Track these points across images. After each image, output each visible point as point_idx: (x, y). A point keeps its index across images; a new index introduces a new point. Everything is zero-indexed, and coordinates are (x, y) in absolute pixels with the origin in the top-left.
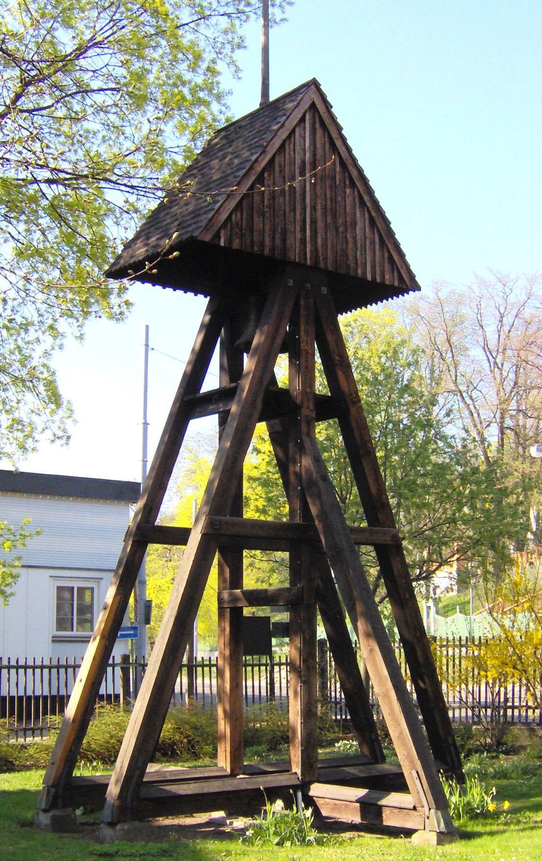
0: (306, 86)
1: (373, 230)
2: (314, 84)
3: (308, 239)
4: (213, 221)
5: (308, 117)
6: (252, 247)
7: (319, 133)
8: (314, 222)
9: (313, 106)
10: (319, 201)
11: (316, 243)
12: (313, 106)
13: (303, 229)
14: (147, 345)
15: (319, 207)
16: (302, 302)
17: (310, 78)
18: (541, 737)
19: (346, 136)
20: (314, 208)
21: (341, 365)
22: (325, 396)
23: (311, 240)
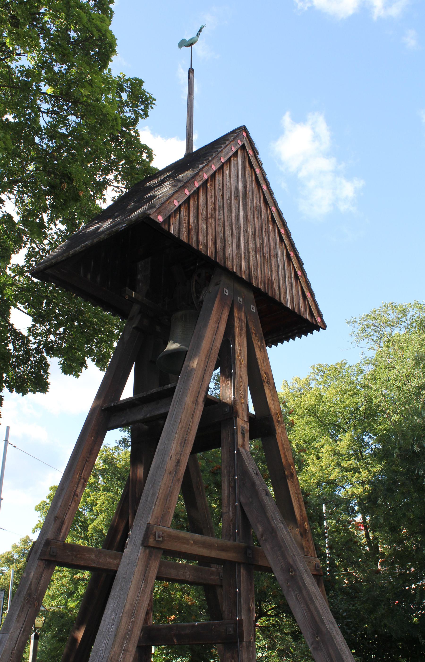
0: (239, 128)
1: (282, 244)
2: (244, 129)
3: (243, 256)
4: (164, 207)
5: (239, 153)
6: (198, 246)
7: (248, 168)
8: (247, 243)
9: (243, 147)
10: (249, 225)
11: (249, 262)
12: (243, 147)
13: (239, 246)
14: (6, 441)
15: (250, 230)
16: (236, 314)
17: (242, 125)
18: (300, 661)
19: (259, 150)
20: (246, 231)
21: (267, 382)
22: (220, 369)
23: (245, 258)
